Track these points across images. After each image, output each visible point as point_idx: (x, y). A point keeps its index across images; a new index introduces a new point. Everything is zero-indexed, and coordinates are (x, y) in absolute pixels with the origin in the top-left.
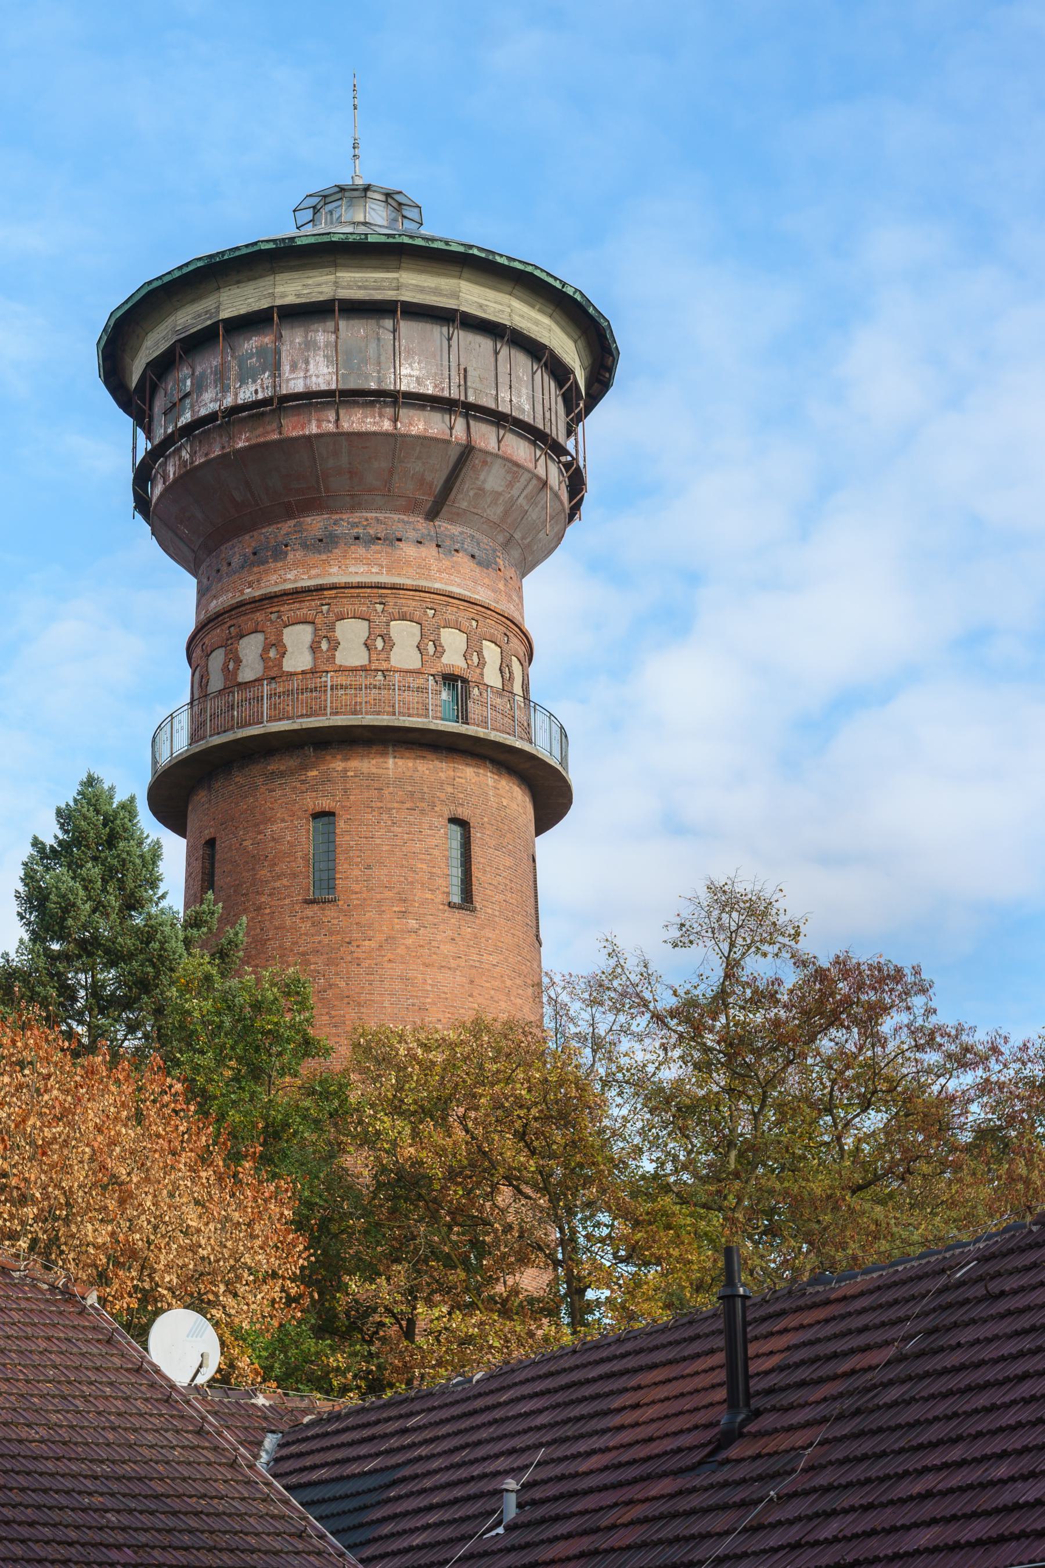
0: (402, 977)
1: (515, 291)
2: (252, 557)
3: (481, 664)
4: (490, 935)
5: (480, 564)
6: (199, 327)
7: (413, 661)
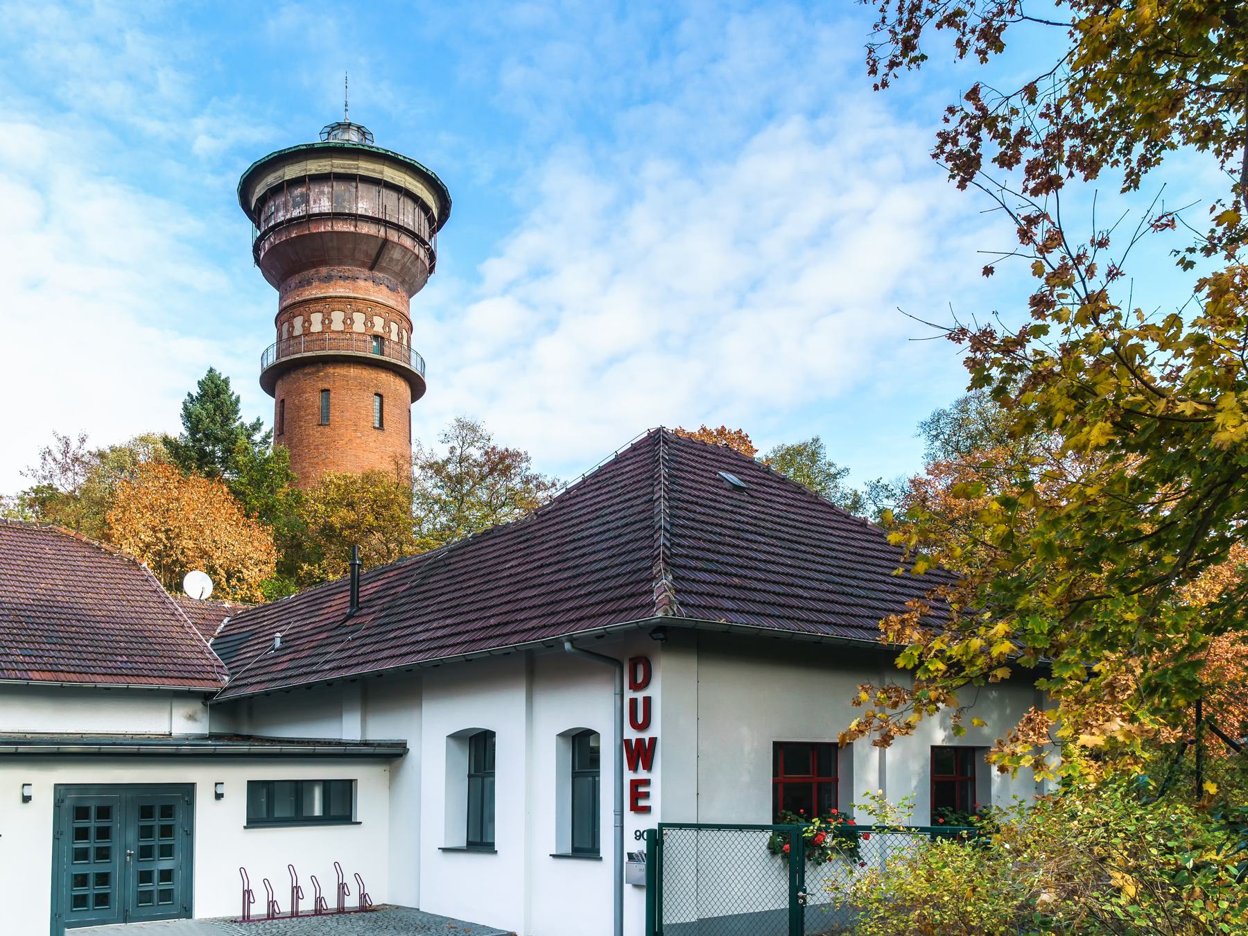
0: (354, 453)
3: (390, 331)
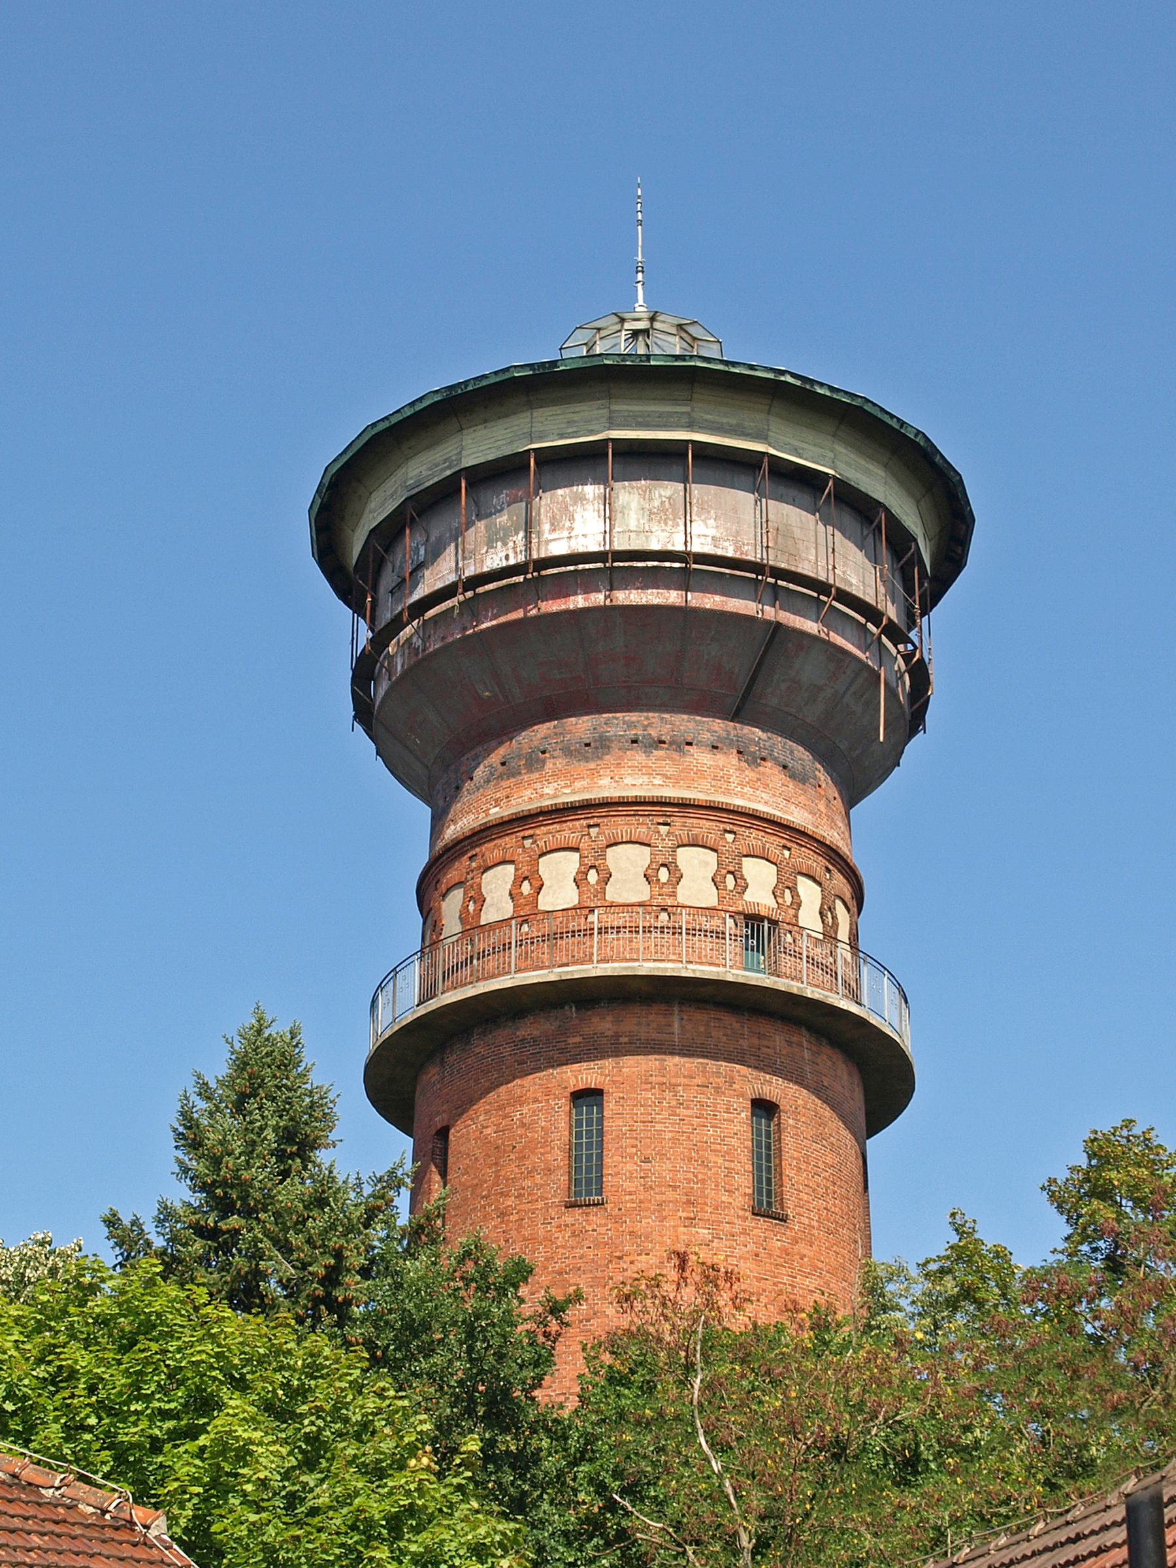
1: (840, 433)
2: (501, 769)
3: (797, 904)
4: (805, 1252)
5: (793, 776)
6: (436, 479)
7: (710, 898)
